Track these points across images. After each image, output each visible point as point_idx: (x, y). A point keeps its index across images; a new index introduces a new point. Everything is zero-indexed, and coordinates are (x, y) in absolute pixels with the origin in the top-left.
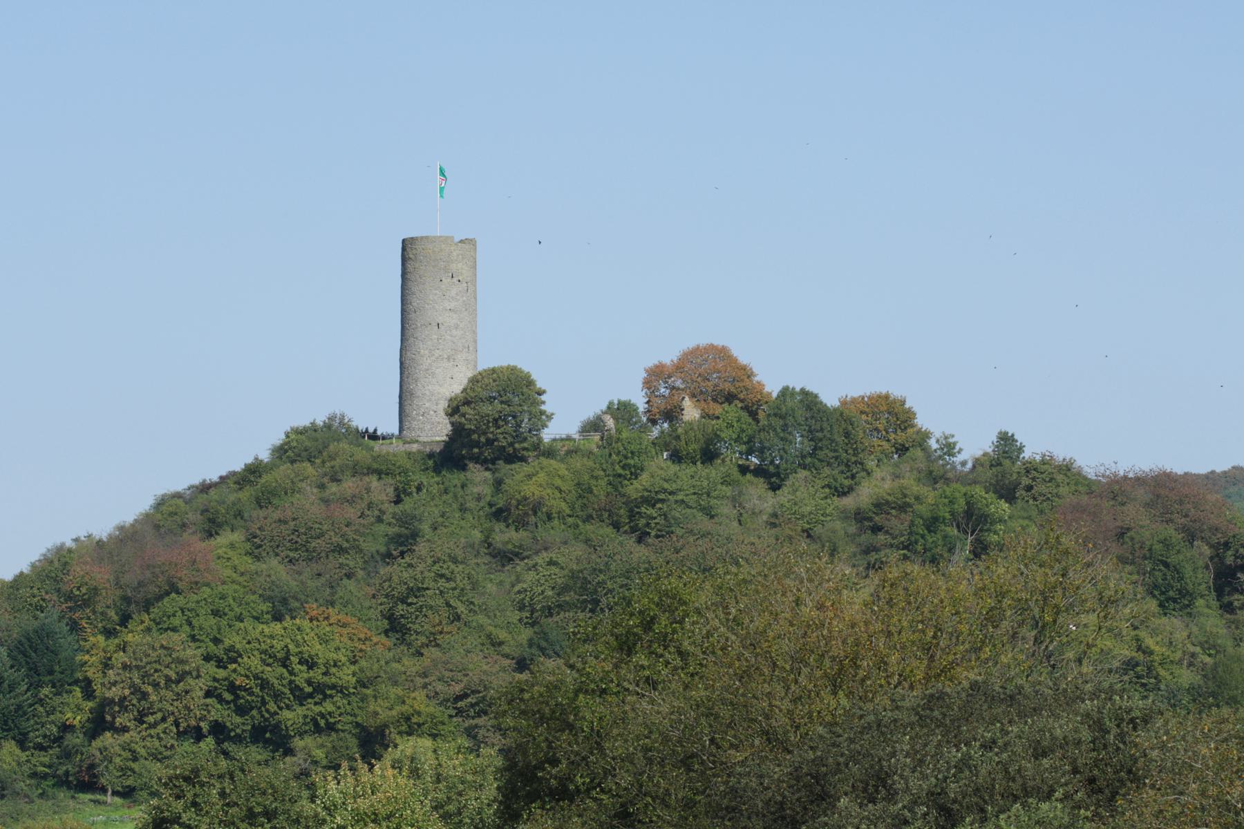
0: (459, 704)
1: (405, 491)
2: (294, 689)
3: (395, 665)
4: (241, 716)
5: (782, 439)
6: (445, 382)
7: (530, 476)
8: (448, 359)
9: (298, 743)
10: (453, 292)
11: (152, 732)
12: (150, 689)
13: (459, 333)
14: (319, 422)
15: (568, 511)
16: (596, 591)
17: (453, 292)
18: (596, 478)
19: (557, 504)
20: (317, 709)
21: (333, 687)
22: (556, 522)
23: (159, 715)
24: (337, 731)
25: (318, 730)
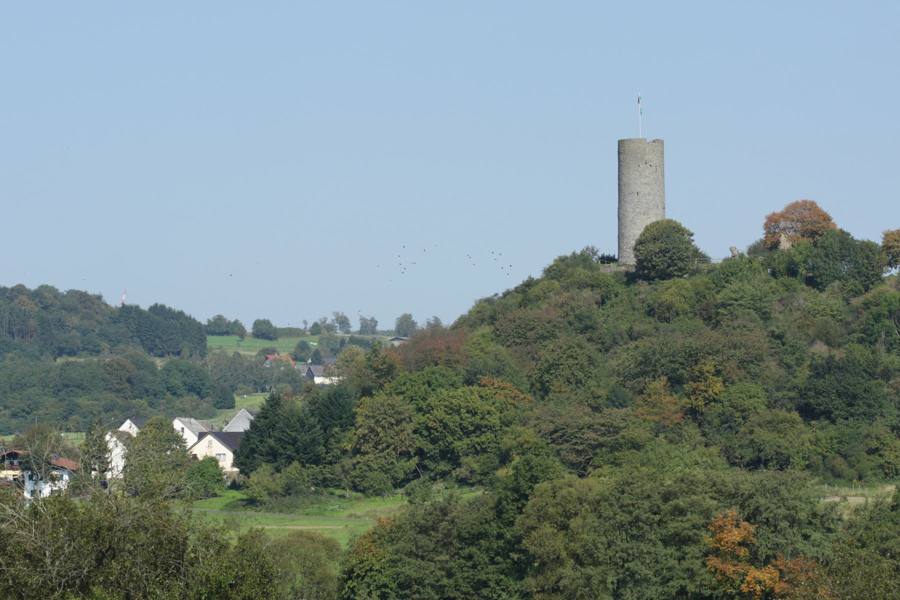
0: (554, 436)
1: (607, 297)
2: (462, 428)
3: (529, 412)
4: (434, 444)
5: (825, 262)
6: (635, 232)
7: (667, 289)
8: (644, 214)
9: (464, 460)
10: (647, 173)
11: (381, 454)
12: (379, 429)
13: (651, 197)
14: (578, 252)
15: (689, 310)
16: (655, 366)
17: (647, 173)
18: (709, 289)
19: (681, 305)
20: (478, 440)
21: (486, 426)
22: (682, 316)
23: (385, 445)
24: (487, 452)
25: (477, 453)
